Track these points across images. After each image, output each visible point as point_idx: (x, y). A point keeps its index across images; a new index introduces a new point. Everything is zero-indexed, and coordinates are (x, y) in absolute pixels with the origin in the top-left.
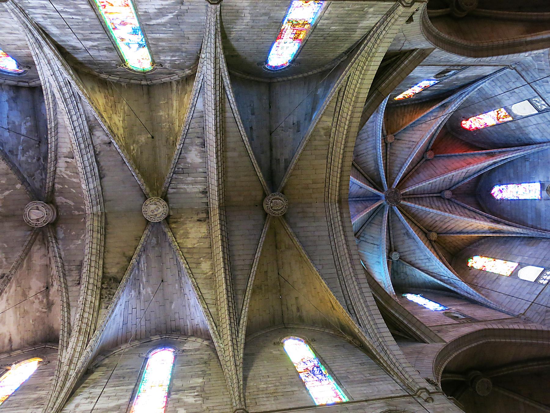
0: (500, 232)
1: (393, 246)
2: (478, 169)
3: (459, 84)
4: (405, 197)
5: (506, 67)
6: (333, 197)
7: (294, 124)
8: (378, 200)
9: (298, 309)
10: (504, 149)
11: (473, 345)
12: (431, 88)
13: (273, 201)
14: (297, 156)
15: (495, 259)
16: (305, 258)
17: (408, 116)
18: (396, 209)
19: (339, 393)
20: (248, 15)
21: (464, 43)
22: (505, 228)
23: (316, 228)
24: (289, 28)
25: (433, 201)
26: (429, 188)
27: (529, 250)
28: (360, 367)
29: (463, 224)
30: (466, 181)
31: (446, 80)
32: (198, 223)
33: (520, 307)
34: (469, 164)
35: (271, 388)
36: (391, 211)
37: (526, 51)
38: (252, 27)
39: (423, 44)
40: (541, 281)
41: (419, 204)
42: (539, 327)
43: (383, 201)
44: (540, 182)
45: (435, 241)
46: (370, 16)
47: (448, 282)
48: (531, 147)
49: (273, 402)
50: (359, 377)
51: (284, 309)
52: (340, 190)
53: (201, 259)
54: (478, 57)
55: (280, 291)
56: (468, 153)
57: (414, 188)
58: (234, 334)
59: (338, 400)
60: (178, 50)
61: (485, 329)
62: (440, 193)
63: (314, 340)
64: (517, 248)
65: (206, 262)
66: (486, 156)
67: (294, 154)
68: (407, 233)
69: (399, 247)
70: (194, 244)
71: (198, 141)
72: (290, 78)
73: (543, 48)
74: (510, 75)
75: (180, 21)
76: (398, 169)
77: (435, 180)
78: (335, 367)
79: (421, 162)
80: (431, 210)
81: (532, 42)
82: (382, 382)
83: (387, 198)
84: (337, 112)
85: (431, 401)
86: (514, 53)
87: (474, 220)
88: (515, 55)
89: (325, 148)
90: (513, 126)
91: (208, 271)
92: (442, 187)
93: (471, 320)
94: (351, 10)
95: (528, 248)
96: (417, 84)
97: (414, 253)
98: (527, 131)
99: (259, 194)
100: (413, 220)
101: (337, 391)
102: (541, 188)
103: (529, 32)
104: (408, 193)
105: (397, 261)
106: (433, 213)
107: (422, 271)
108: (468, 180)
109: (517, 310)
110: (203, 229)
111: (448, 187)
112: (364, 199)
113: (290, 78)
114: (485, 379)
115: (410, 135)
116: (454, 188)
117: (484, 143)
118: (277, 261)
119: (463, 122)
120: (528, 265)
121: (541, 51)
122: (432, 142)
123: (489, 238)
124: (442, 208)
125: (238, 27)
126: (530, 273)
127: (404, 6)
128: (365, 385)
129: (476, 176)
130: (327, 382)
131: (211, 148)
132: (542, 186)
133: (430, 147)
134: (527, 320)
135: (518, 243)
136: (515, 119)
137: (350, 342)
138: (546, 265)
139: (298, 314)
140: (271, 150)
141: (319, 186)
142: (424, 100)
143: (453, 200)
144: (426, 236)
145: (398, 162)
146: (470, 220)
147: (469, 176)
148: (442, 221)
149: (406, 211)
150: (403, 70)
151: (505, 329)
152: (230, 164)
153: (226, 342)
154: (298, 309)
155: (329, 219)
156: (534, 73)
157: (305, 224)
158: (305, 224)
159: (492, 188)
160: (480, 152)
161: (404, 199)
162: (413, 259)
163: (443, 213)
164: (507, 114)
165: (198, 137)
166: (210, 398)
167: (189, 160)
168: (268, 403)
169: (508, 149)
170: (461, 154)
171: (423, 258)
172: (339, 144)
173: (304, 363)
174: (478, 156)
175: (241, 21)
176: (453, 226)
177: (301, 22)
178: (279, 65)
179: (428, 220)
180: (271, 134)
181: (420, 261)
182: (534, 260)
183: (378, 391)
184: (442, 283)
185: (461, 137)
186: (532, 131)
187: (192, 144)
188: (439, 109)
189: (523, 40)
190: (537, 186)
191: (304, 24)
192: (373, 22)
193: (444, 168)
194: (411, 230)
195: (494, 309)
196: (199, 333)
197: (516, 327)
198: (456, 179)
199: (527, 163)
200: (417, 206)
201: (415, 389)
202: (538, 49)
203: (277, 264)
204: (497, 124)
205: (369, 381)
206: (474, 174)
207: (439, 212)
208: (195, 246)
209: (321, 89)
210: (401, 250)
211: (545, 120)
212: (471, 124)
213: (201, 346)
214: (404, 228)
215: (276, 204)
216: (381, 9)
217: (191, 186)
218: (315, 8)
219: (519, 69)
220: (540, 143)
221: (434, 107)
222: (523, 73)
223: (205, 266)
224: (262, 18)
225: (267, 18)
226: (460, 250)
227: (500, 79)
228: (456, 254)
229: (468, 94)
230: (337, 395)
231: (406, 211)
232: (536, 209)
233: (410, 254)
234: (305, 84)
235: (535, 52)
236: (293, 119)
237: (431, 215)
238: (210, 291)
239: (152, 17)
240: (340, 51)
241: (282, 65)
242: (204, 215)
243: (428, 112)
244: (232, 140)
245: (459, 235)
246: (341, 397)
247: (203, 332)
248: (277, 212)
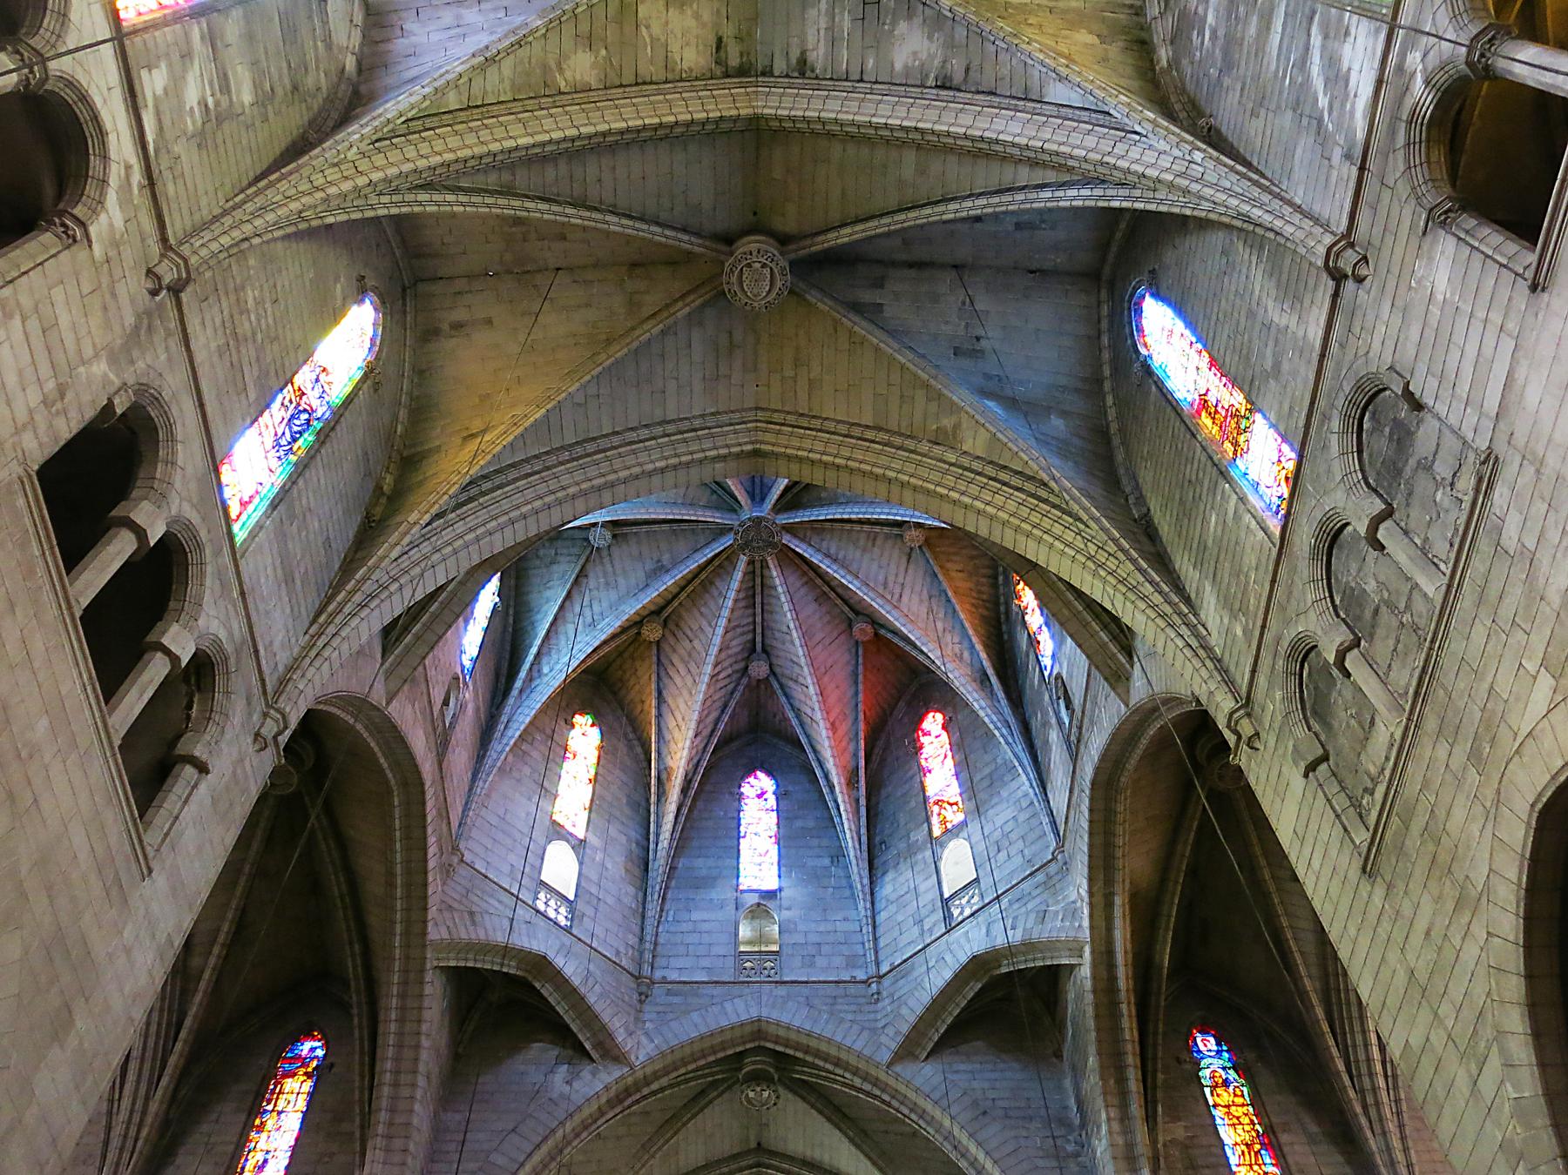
0: (662, 794)
1: (626, 530)
2: (818, 747)
3: (1035, 724)
4: (758, 565)
5: (1060, 846)
6: (769, 437)
7: (978, 339)
8: (752, 496)
9: (458, 326)
10: (863, 811)
11: (382, 760)
12: (1032, 657)
13: (767, 271)
14: (889, 347)
15: (595, 781)
16: (603, 356)
17: (969, 585)
18: (728, 541)
19: (251, 507)
20: (1284, 322)
21: (1132, 764)
22: (669, 818)
23: (686, 384)
24: (1232, 401)
25: (743, 634)
26: (778, 626)
27: (616, 865)
28: (320, 541)
29: (682, 706)
30: (791, 715)
31: (1047, 697)
32: (713, 42)
33: (475, 850)
34: (833, 727)
35: (247, 325)
36: (723, 530)
37: (1091, 894)
38: (1251, 314)
39: (1139, 690)
40: (542, 895)
41: (736, 601)
42: (433, 901)
43: (748, 512)
44: (780, 889)
45: (639, 634)
46: (1226, 621)
47: (535, 674)
48: (866, 873)
49: (213, 345)
50: (295, 548)
51: (460, 284)
52: (789, 458)
53: (603, 52)
54: (1092, 789)
55: (510, 272)
56: (862, 726)
57: (780, 589)
58: (390, 187)
59: (234, 511)
60: (1228, 65)
61: (423, 785)
62: (764, 650)
63: (376, 387)
64: (622, 837)
65: (594, 66)
66: (850, 768)
67: (892, 333)
68: (660, 570)
69: (625, 547)
70: (648, 27)
71: (956, 67)
72: (1105, 340)
73: (1092, 927)
74: (1039, 845)
75: (1305, 121)
76: (833, 551)
77: (797, 642)
78: (318, 474)
79: (846, 609)
80: (720, 631)
81: (1109, 905)
82: (288, 611)
83: (757, 521)
84: (999, 472)
85: (257, 747)
86: (1090, 868)
87: (691, 733)
88: (1086, 870)
89: (904, 424)
90: (919, 835)
91: (568, 74)
93: (442, 745)
94: (1247, 583)
95: (620, 859)
96: (1047, 624)
97: (607, 584)
98: (902, 866)
99: (788, 222)
100: (697, 581)
101: (257, 500)
102: (768, 892)
103: (1134, 898)
104: (766, 572)
105: (587, 539)
106: (712, 635)
107: (562, 607)
108: (794, 722)
109: (471, 844)
110: (692, 57)
111: (777, 670)
113: (1105, 340)
114: (295, 780)
115: (918, 588)
116: (776, 685)
117: (883, 760)
118: (595, 266)
119: (939, 716)
120: (581, 864)
121: (1086, 923)
122: (896, 640)
123: (645, 764)
124: (723, 655)
125: (1259, 277)
126: (560, 867)
127: (1231, 714)
128: (279, 571)
129: (803, 740)
130: (274, 463)
131: (932, 114)
132: (771, 895)
133: (882, 632)
134: (447, 871)
135: (633, 834)
136: (936, 844)
137: (379, 488)
138: (580, 906)
139: (445, 327)
140: (910, 265)
141: (803, 395)
142: (1004, 628)
143: (745, 681)
144: (652, 613)
145: (852, 553)
146: (693, 725)
147: (802, 724)
148: (690, 655)
149: (719, 566)
150: (1086, 625)
151: (425, 827)
152: (880, 153)
153: (363, 165)
154: (458, 326)
155: (710, 422)
156: (1038, 900)
157: (697, 347)
158: (697, 347)
159: (769, 773)
160: (862, 754)
161: (751, 562)
162: (592, 583)
163: (711, 659)
164: (949, 826)
165: (967, 70)
166: (204, 152)
167: (903, 26)
168: (209, 331)
169: (863, 820)
170: (860, 706)
171: (596, 608)
172: (910, 468)
173: (317, 380)
174: (851, 747)
175: (1273, 292)
176: (678, 680)
177: (1242, 439)
178: (1144, 322)
179: (693, 621)
180: (955, 267)
182: (595, 877)
183: (267, 613)
184: (530, 658)
185: (902, 704)
186: (902, 879)
187: (950, 45)
188: (977, 665)
189: (1118, 888)
190: (771, 883)
191: (1236, 444)
192: (1210, 620)
194: (668, 582)
195: (470, 790)
196: (376, 34)
197: (432, 851)
198: (797, 692)
199: (827, 861)
200: (732, 595)
201: (281, 704)
202: (1091, 916)
203: (584, 267)
204: (925, 799)
205: (289, 579)
206: (808, 736)
207: (714, 650)
208: (643, 29)
209: (1063, 427)
210: (616, 551)
211: (924, 912)
212: (934, 734)
213: (340, 49)
214: (675, 564)
215: (758, 274)
216: (1235, 652)
217: (823, 25)
218: (1268, 491)
219: (1053, 868)
220: (872, 894)
221: (983, 655)
222: (1040, 877)
223: (582, 66)
224: (1269, 352)
225: (1268, 364)
226: (615, 693)
227: (1034, 822)
228: (603, 688)
229: (1008, 743)
230: (244, 504)
231: (719, 566)
232: (715, 879)
233: (605, 574)
234: (1084, 380)
235: (1086, 911)
236: (993, 337)
237: (709, 630)
238: (507, 83)
239: (1330, 43)
240: (1154, 505)
241: (1141, 330)
242: (734, 61)
243: (975, 640)
244: (955, 173)
245: (654, 694)
246: (243, 518)
247: (382, 47)
248: (734, 279)
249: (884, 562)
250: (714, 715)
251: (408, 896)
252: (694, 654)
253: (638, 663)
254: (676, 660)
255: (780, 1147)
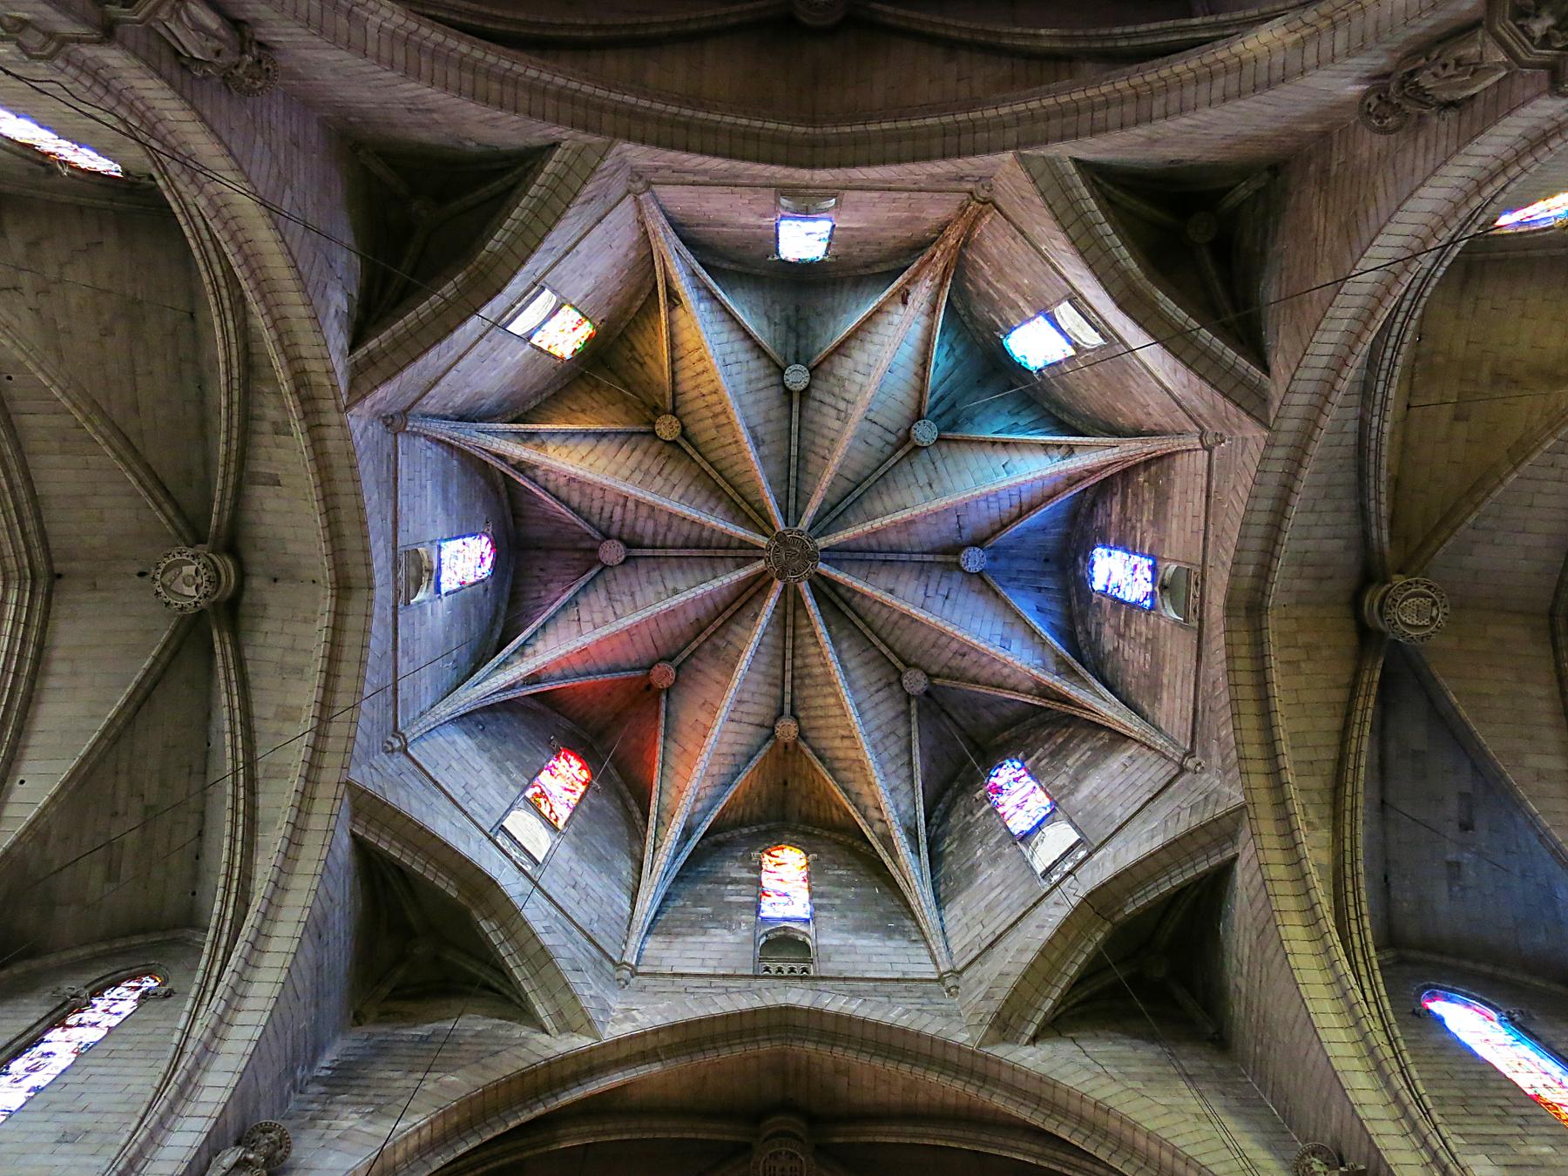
13: (1426, 622)
69: (777, 403)
81: (645, 1057)
92: (626, 575)
106: (673, 500)
112: (870, 556)
149: (746, 509)
162: (754, 365)
176: (621, 457)
181: (743, 357)
193: (636, 638)
226: (582, 376)
233: (758, 380)
237: (675, 495)
248: (1422, 589)
249: (757, 698)
250: (575, 499)
251: (674, 122)
252: (648, 479)
253: (620, 405)
254: (637, 454)
255: (60, 609)
